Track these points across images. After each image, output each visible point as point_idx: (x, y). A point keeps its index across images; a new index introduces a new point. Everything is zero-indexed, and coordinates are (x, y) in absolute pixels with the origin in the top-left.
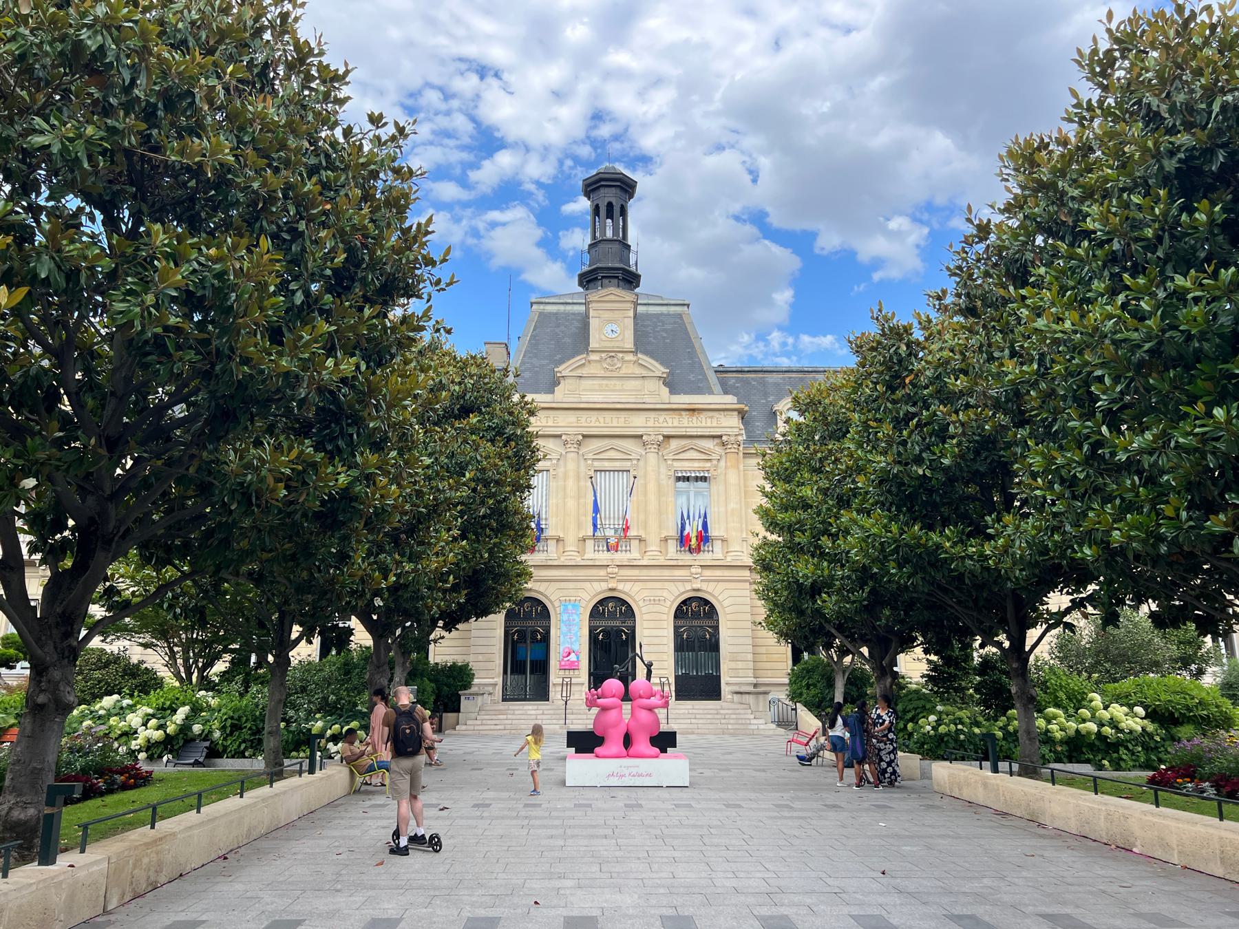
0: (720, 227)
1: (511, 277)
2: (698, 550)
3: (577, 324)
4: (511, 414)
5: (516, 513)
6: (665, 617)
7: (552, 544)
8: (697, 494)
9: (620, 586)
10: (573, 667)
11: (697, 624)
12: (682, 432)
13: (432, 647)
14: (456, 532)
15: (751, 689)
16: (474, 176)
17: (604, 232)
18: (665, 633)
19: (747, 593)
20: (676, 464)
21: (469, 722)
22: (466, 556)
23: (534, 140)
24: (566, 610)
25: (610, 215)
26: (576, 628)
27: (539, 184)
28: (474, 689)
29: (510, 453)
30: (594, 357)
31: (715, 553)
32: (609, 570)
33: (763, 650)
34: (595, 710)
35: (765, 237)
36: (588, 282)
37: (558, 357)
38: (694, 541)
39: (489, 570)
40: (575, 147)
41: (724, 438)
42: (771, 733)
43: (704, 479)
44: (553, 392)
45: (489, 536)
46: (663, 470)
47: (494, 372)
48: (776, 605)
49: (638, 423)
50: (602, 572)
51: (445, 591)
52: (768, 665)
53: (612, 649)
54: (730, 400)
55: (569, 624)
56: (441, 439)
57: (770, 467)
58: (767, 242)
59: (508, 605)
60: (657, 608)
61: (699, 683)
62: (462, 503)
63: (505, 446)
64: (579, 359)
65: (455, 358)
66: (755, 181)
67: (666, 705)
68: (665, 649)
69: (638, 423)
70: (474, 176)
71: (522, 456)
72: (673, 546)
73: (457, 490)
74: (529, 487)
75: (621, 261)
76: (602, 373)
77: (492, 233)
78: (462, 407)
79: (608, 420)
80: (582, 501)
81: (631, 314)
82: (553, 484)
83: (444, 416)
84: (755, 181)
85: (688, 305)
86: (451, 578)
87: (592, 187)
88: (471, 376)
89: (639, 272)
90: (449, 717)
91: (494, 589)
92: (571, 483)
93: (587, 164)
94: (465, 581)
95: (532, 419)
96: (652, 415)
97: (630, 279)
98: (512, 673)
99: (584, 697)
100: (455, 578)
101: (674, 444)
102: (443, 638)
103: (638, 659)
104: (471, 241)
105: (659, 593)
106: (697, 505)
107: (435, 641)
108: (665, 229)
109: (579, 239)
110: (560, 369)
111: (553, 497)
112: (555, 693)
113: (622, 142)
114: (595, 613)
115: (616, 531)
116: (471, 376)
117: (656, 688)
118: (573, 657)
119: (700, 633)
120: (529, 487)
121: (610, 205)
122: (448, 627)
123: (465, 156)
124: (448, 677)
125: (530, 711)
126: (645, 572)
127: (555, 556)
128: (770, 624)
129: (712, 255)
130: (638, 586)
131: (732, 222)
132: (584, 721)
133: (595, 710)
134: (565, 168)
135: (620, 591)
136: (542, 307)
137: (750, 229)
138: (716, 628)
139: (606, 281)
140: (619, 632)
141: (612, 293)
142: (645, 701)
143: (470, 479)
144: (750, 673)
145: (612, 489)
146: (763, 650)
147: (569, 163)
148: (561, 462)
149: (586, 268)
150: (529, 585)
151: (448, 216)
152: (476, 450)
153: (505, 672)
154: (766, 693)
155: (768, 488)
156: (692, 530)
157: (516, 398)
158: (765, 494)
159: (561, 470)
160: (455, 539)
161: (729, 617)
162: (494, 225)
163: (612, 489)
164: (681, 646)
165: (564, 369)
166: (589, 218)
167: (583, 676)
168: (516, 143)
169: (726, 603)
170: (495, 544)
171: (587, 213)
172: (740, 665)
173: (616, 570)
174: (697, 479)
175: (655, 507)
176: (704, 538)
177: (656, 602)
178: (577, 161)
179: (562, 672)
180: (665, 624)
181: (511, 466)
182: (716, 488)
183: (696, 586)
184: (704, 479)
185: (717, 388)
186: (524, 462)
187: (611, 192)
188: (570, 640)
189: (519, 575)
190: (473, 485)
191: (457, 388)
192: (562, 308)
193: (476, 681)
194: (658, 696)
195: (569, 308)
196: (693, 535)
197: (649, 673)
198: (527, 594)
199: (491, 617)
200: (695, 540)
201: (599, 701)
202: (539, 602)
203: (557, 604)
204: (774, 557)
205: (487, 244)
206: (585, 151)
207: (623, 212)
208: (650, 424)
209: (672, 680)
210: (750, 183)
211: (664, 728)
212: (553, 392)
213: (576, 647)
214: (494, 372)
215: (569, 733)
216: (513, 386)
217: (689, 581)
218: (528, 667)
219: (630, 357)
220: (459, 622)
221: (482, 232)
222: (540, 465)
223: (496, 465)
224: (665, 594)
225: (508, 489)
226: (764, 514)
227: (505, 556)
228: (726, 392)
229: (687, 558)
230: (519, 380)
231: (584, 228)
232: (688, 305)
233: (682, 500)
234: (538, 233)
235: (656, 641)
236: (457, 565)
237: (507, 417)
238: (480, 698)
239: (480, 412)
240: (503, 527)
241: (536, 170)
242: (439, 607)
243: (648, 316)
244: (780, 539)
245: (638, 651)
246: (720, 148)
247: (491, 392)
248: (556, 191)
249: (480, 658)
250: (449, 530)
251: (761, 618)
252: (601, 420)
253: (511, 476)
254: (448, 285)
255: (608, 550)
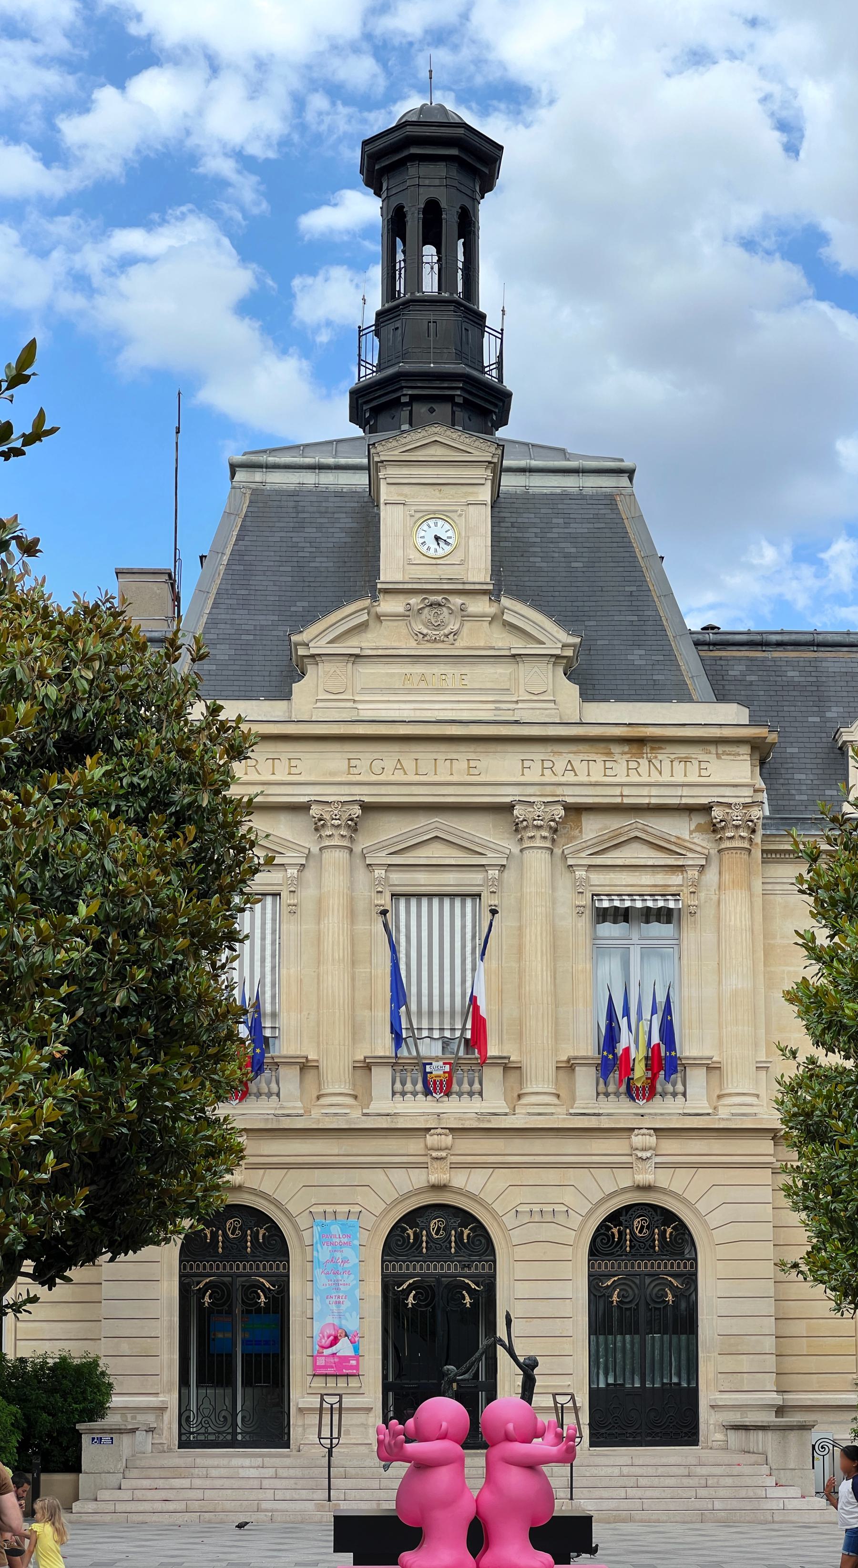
0: (707, 265)
1: (173, 402)
2: (650, 1092)
3: (346, 521)
4: (185, 754)
5: (202, 1000)
6: (568, 1253)
7: (289, 1080)
8: (647, 952)
9: (459, 1180)
10: (344, 1370)
11: (644, 1271)
12: (611, 797)
13: (9, 1320)
14: (57, 1049)
15: (769, 1418)
16: (74, 130)
17: (416, 279)
18: (566, 1290)
19: (767, 1194)
20: (597, 878)
21: (103, 1495)
22: (83, 1107)
23: (230, 43)
24: (326, 1237)
25: (432, 236)
26: (351, 1280)
27: (245, 161)
28: (111, 1420)
29: (184, 854)
30: (389, 605)
31: (693, 1100)
32: (431, 1140)
33: (799, 1328)
34: (400, 1469)
35: (821, 297)
36: (377, 411)
37: (300, 606)
38: (639, 1072)
39: (141, 1140)
40: (336, 62)
41: (717, 813)
42: (814, 1517)
43: (665, 916)
44: (286, 696)
45: (137, 1059)
46: (566, 895)
47: (141, 647)
48: (834, 1221)
49: (502, 773)
50: (414, 1146)
51: (36, 1190)
52: (812, 1364)
53: (439, 1325)
54: (732, 715)
55: (335, 1269)
56: (17, 820)
57: (827, 887)
58: (824, 307)
59: (187, 1223)
60: (547, 1232)
61: (648, 1396)
62: (70, 978)
63: (172, 835)
64: (352, 612)
65: (45, 613)
66: (792, 149)
67: (568, 1457)
68: (567, 1327)
69: (502, 773)
70: (74, 130)
71: (214, 862)
72: (586, 1080)
73: (57, 946)
74: (232, 937)
75: (460, 356)
76: (409, 646)
77: (123, 283)
78: (66, 737)
79: (426, 766)
80: (362, 970)
81: (485, 494)
82: (289, 927)
83: (21, 761)
84: (792, 149)
85: (630, 473)
86: (50, 1157)
87: (387, 160)
88: (87, 661)
89: (508, 384)
90: (55, 1482)
91: (152, 1185)
92: (334, 926)
93: (365, 102)
94: (84, 1166)
95: (237, 767)
96: (537, 753)
97: (485, 405)
98: (200, 1382)
99: (373, 1438)
100: (59, 1159)
101: (593, 828)
102: (34, 1300)
103: (501, 1352)
104: (71, 302)
105: (553, 1195)
106: (648, 980)
107: (17, 1308)
108: (576, 270)
109: (350, 298)
110: (305, 636)
111: (297, 959)
112: (303, 1430)
113: (455, 48)
114: (399, 1243)
115: (446, 1043)
116: (87, 661)
117: (546, 1419)
118: (344, 1348)
119: (652, 1289)
120: (232, 937)
121: (432, 210)
122: (46, 1276)
123: (52, 79)
124: (52, 1391)
125: (243, 1468)
126: (518, 1145)
127: (295, 1105)
128: (818, 1266)
129: (681, 340)
130: (501, 1179)
131: (739, 253)
132: (374, 1492)
133: (400, 1469)
134: (310, 116)
135: (460, 1192)
136: (258, 476)
137: (784, 274)
138: (691, 1279)
139: (421, 409)
140: (456, 1288)
141: (440, 440)
142: (519, 1448)
143: (89, 920)
144: (769, 1382)
145: (436, 942)
146: (799, 1328)
147: (319, 102)
148: (309, 874)
149: (368, 374)
150: (237, 1177)
151: (13, 235)
152: (103, 846)
153: (184, 1381)
154: (804, 1427)
155: (822, 938)
156: (634, 1041)
157: (197, 712)
158: (815, 953)
159: (308, 894)
160: (56, 1065)
161: (721, 1252)
162: (127, 262)
163: (436, 942)
164: (605, 1320)
165: (315, 637)
166: (376, 247)
167: (369, 1390)
168: (185, 50)
169: (714, 1220)
170: (153, 1078)
171: (366, 232)
172: (745, 1363)
173: (448, 1140)
174: (649, 915)
175: (546, 982)
176: (665, 1062)
177: (546, 1216)
178: (336, 92)
179: (319, 1383)
180: (566, 1269)
181: (187, 885)
182: (695, 938)
183: (643, 1178)
184: (665, 916)
185: (699, 683)
186: (218, 872)
187: (432, 174)
188: (337, 1303)
189: (212, 1153)
190: (95, 932)
191: (52, 691)
192: (309, 479)
193: (116, 1401)
194: (550, 1436)
195: (327, 479)
196: (638, 1055)
197: (528, 1390)
198: (232, 1199)
199: (148, 1251)
200: (641, 1063)
201: (410, 1447)
202: (261, 1218)
203: (303, 1222)
204: (835, 1108)
205: (111, 311)
206: (361, 71)
207: (467, 227)
208: (530, 777)
209: (583, 1400)
210: (779, 149)
211: (563, 1507)
212: (286, 696)
213: (351, 1325)
214: (141, 647)
215: (337, 1519)
216: (191, 685)
217: (628, 1166)
218: (238, 1367)
219: (481, 606)
220: (71, 1262)
221: (97, 280)
222: (261, 881)
223: (151, 884)
224: (569, 1197)
225: (181, 943)
226: (810, 1001)
227: (178, 1107)
228: (721, 697)
229: (620, 1110)
230: (205, 666)
231: (358, 266)
232: (630, 473)
233: (610, 968)
234: (241, 279)
235: (544, 1306)
236: (63, 1127)
237: (175, 761)
238: (126, 1439)
239: (109, 750)
240: (171, 1037)
241: (237, 121)
242: (22, 1226)
243: (528, 499)
244: (850, 1064)
245: (501, 1331)
246: (698, 58)
247: (135, 699)
248: (288, 176)
249: (125, 1347)
250: (42, 1043)
251: (798, 1254)
252: (408, 764)
253: (187, 909)
254: (30, 439)
255: (427, 1092)
